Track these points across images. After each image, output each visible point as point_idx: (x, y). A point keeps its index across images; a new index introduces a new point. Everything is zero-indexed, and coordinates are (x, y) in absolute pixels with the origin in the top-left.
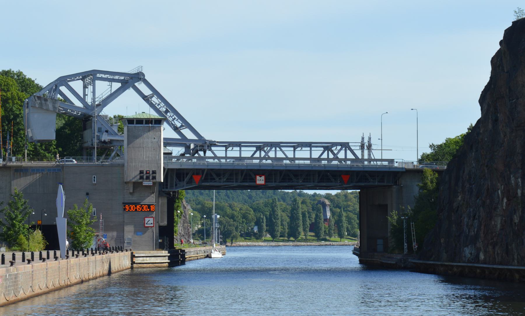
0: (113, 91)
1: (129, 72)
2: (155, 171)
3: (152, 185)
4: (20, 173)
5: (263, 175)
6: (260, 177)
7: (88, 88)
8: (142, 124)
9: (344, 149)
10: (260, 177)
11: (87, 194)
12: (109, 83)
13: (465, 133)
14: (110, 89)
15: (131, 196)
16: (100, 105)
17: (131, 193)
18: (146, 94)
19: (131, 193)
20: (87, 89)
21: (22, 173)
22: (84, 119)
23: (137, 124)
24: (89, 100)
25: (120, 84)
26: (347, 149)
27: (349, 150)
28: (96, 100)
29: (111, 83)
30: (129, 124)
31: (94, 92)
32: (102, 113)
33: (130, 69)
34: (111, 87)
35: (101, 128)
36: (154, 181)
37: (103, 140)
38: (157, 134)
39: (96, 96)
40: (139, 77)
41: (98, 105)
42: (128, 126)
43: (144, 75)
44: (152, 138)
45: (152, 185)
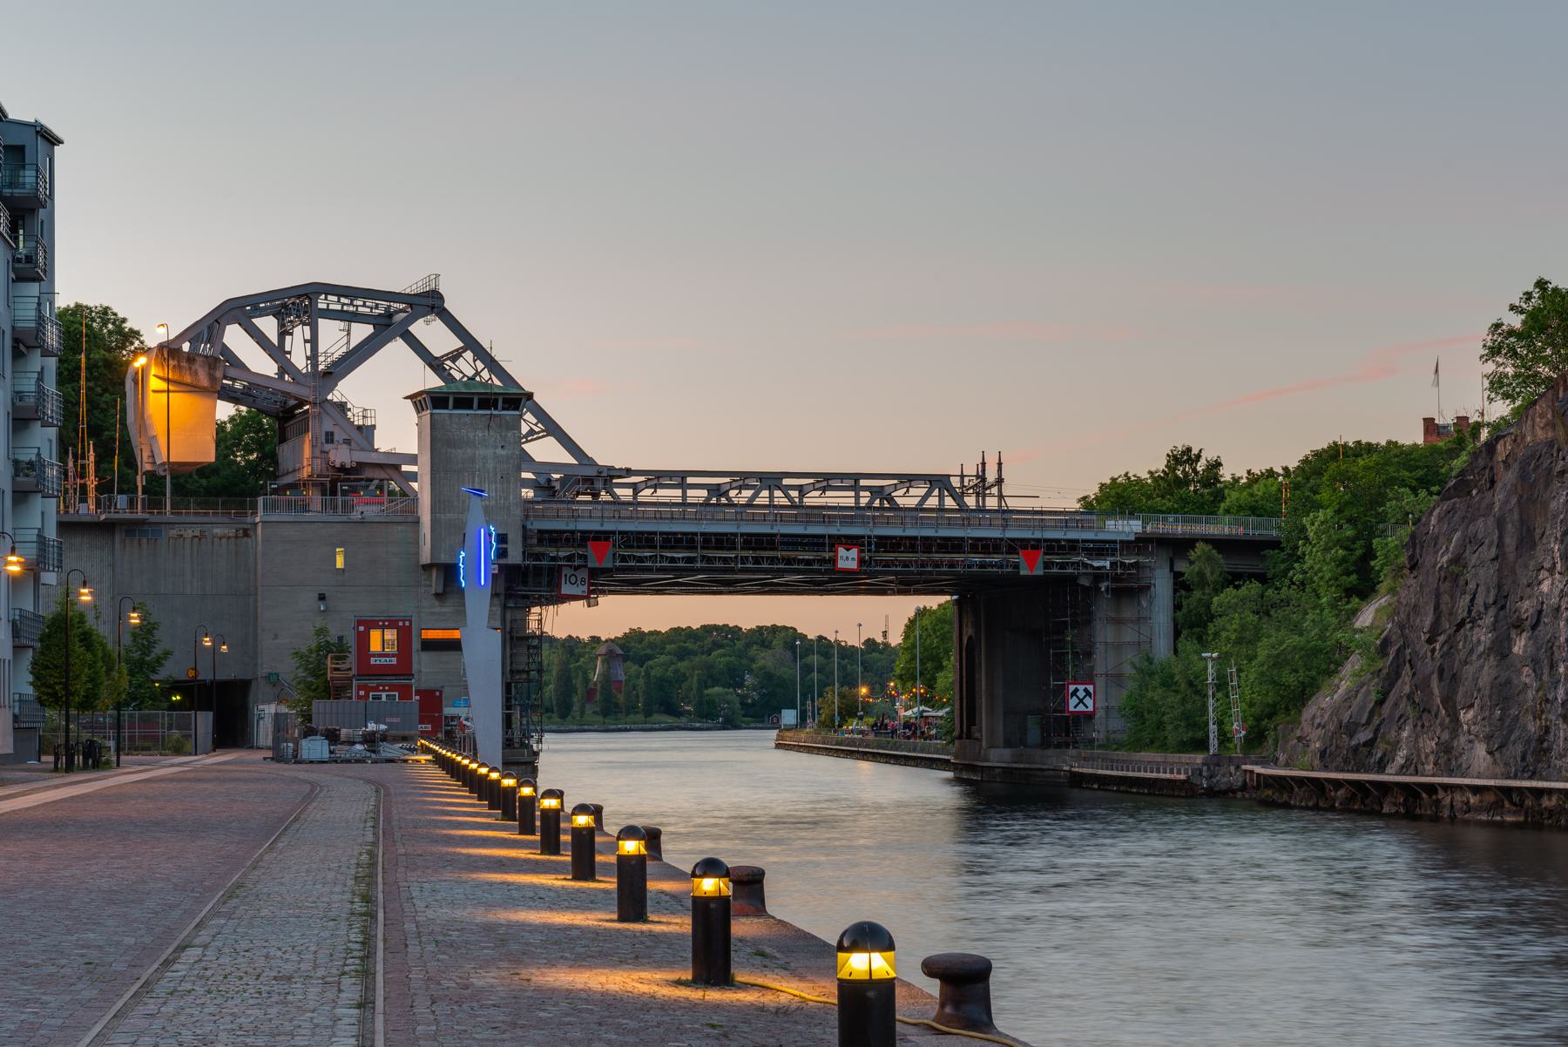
0: (353, 344)
1: (408, 291)
2: (506, 535)
3: (210, 715)
4: (140, 540)
5: (855, 545)
6: (848, 550)
7: (291, 334)
8: (471, 408)
9: (936, 492)
10: (848, 550)
11: (322, 598)
12: (342, 323)
13: (1144, 475)
14: (345, 340)
15: (437, 603)
16: (331, 373)
17: (437, 595)
18: (437, 352)
19: (437, 595)
20: (288, 338)
21: (144, 540)
22: (281, 415)
23: (455, 407)
24: (299, 359)
25: (371, 326)
26: (946, 493)
27: (951, 495)
28: (321, 359)
29: (349, 326)
30: (435, 407)
31: (313, 341)
32: (335, 396)
33: (405, 281)
34: (349, 334)
35: (332, 434)
36: (503, 561)
37: (338, 465)
38: (509, 435)
39: (321, 349)
40: (430, 303)
41: (327, 374)
42: (432, 414)
43: (441, 298)
44: (496, 447)
45: (210, 715)
